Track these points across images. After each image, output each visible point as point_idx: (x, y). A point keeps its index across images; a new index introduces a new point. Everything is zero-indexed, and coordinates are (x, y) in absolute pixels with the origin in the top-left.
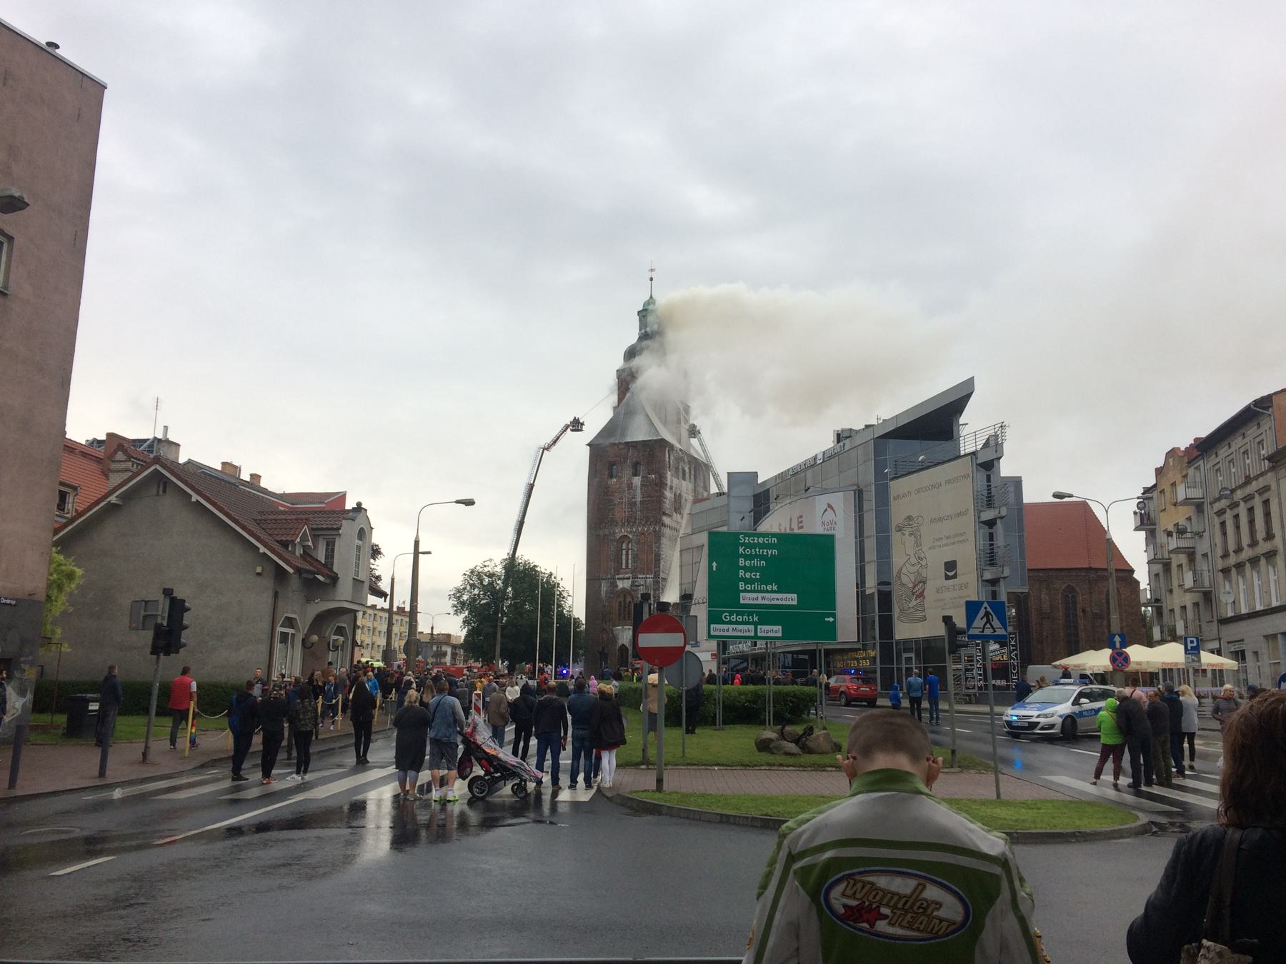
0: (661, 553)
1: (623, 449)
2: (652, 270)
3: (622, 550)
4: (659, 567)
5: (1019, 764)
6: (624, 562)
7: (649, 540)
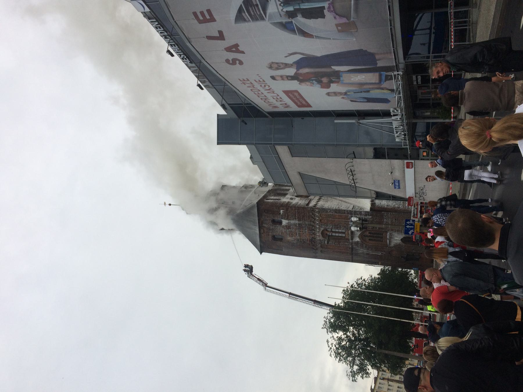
0: (334, 208)
1: (264, 230)
2: (165, 204)
3: (332, 235)
4: (344, 210)
5: (332, 39)
6: (340, 235)
7: (325, 217)
